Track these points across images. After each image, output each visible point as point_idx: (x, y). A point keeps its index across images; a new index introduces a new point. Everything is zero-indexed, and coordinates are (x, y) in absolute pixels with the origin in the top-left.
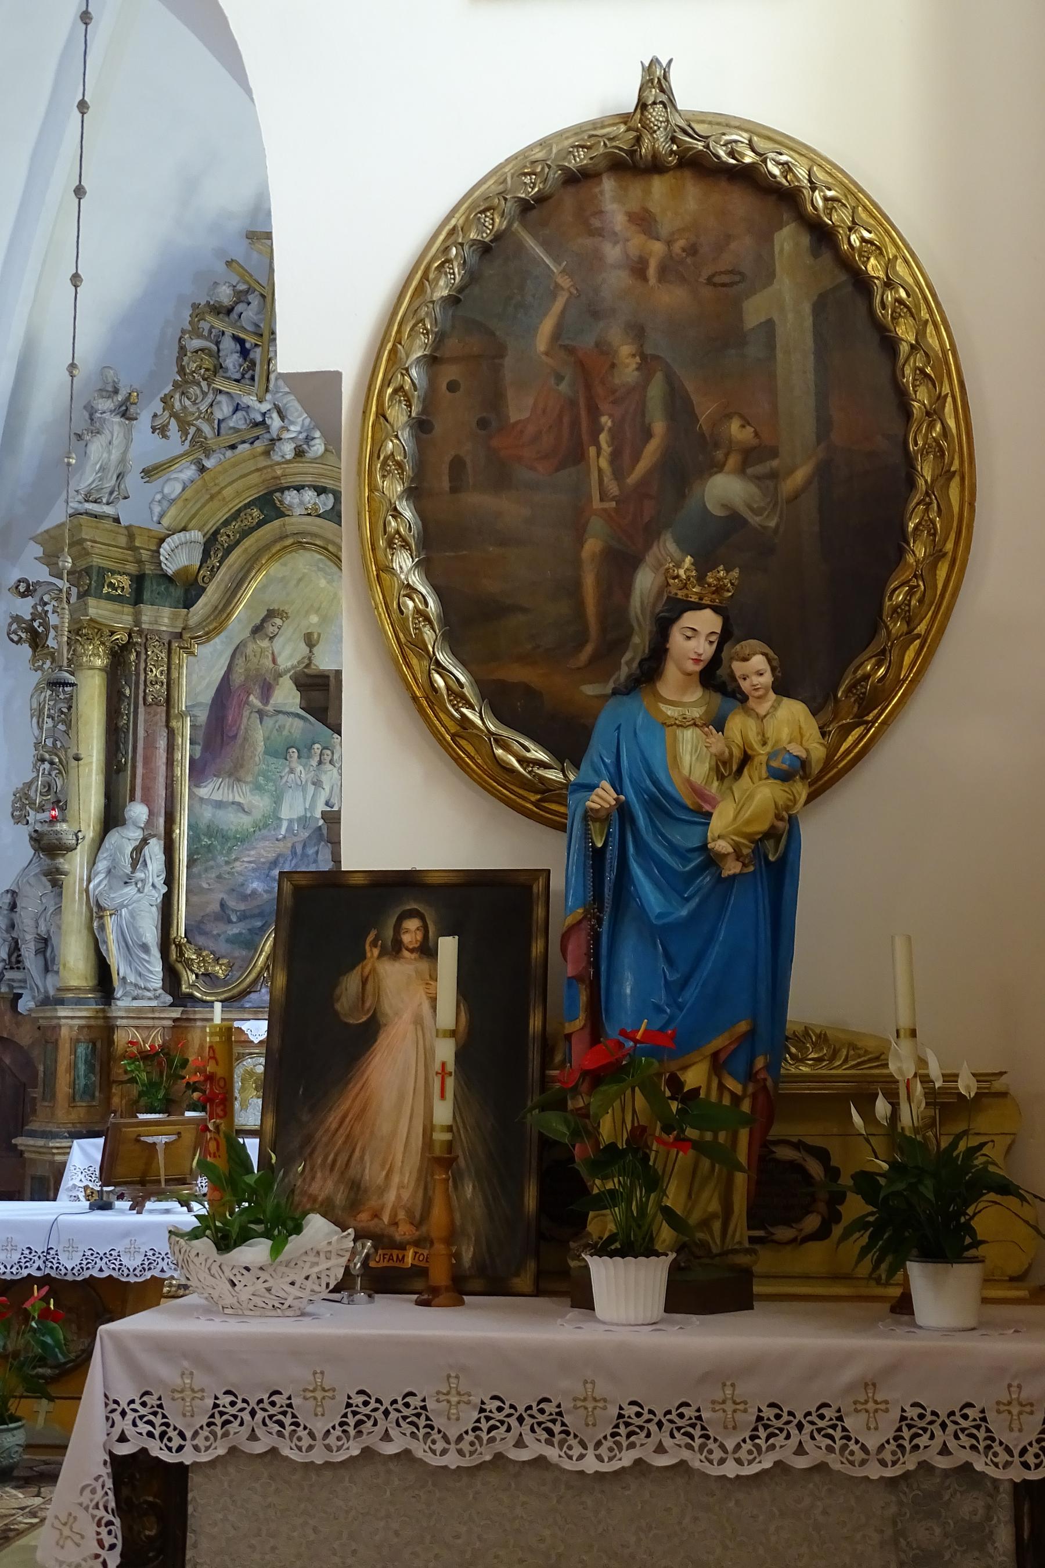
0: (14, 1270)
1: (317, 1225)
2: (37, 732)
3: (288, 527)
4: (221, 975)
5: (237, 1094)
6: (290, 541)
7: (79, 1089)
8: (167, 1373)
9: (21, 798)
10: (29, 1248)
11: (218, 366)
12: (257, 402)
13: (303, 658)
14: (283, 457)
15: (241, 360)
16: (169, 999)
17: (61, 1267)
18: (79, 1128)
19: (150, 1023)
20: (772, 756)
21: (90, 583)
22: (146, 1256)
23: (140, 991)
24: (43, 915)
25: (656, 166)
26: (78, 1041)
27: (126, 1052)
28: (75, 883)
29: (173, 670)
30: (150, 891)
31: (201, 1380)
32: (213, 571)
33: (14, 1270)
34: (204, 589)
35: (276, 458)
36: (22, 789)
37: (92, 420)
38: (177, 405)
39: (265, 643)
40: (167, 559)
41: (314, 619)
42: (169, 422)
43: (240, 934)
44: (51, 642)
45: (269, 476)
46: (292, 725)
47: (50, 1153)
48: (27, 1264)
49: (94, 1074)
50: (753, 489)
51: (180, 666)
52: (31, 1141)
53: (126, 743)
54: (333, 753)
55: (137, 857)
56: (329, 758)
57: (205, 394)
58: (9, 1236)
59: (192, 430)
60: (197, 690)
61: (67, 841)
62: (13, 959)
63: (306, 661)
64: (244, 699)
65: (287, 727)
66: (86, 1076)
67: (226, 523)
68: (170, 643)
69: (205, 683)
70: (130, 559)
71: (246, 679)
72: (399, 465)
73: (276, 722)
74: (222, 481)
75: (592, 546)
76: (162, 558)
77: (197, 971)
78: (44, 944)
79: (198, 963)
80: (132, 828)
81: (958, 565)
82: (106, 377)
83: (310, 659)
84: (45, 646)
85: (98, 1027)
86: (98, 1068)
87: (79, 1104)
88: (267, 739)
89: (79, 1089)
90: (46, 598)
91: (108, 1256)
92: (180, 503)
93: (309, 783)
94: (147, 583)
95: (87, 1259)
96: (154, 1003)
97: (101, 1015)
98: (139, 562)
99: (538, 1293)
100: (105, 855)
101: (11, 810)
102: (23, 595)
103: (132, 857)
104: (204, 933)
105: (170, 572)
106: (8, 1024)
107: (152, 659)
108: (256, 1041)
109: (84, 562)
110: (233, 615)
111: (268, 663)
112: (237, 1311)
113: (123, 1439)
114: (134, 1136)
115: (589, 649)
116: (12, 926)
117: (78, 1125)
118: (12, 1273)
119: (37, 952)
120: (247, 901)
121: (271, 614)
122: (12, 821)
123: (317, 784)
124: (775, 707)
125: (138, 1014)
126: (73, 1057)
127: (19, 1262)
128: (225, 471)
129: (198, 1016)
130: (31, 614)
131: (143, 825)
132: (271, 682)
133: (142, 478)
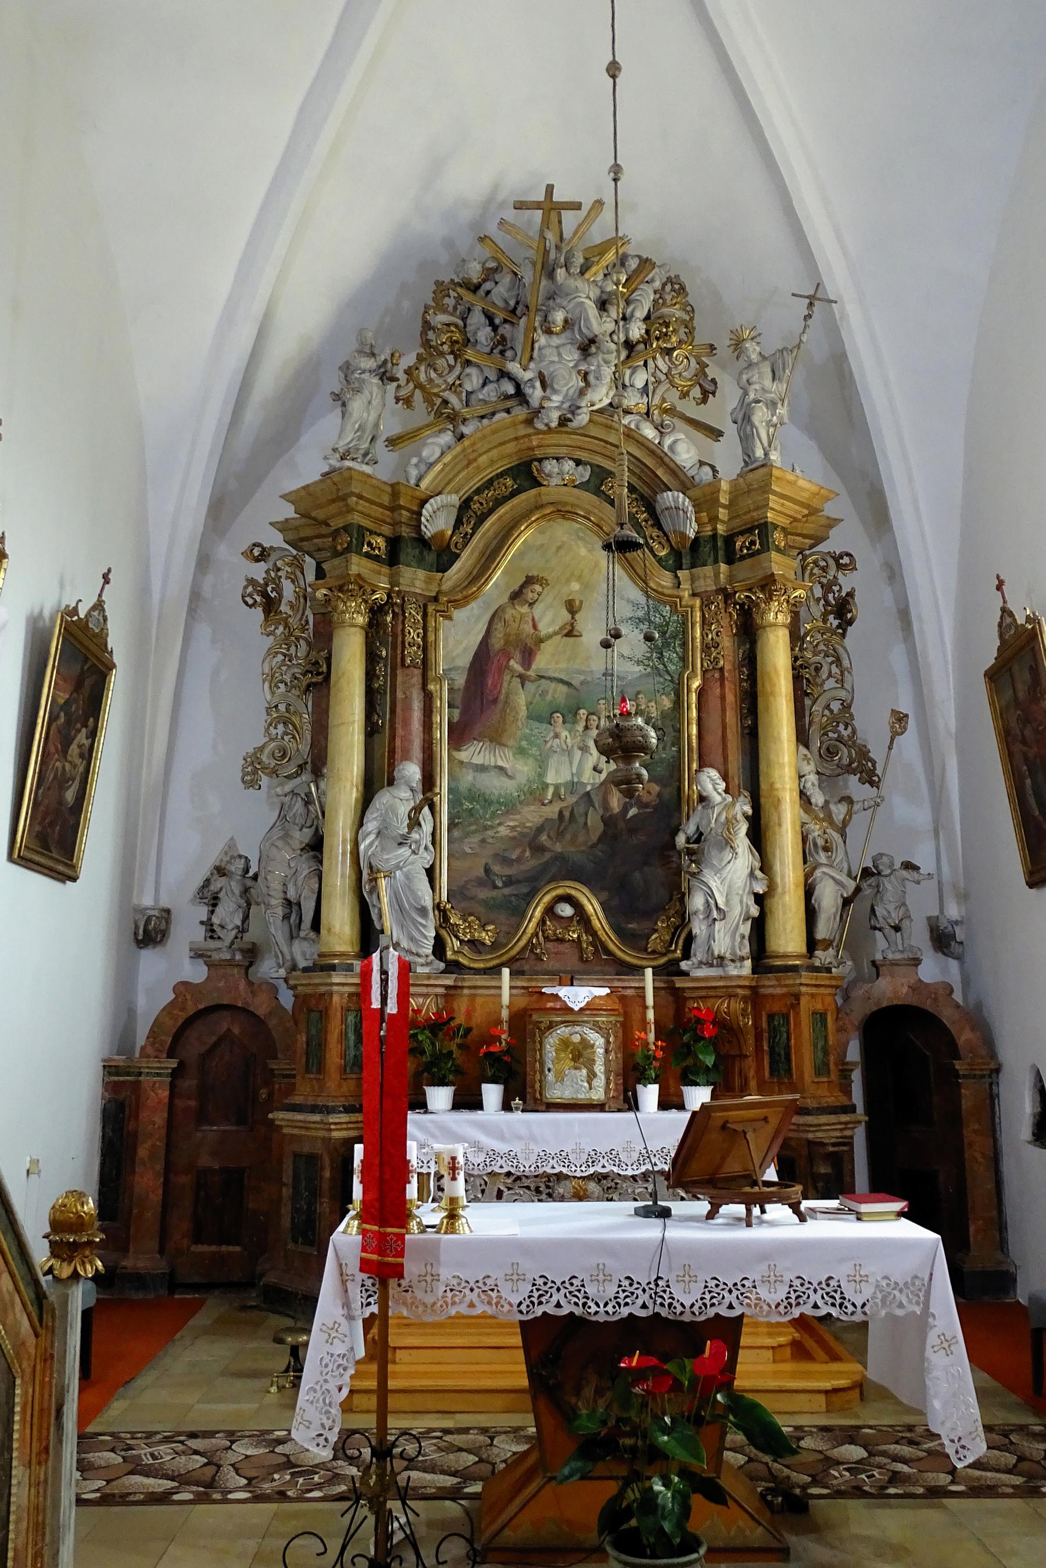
0: (610, 1308)
2: (269, 697)
9: (253, 762)
10: (628, 1278)
16: (442, 966)
17: (675, 1303)
19: (424, 990)
21: (351, 541)
22: (791, 1286)
29: (429, 634)
32: (467, 539)
33: (610, 1308)
34: (458, 556)
36: (255, 753)
38: (423, 377)
39: (525, 609)
41: (575, 586)
42: (413, 394)
44: (284, 608)
46: (555, 690)
48: (627, 1300)
51: (436, 630)
54: (599, 719)
55: (414, 823)
57: (451, 368)
58: (601, 1261)
59: (438, 401)
63: (569, 628)
67: (478, 491)
68: (425, 606)
69: (461, 647)
70: (388, 520)
76: (423, 519)
80: (404, 787)
83: (572, 625)
88: (529, 704)
90: (279, 564)
92: (438, 467)
95: (710, 1292)
102: (257, 560)
106: (243, 993)
108: (576, 1009)
111: (528, 628)
118: (607, 1312)
119: (284, 918)
121: (530, 581)
122: (242, 786)
127: (616, 1298)
128: (484, 437)
129: (466, 984)
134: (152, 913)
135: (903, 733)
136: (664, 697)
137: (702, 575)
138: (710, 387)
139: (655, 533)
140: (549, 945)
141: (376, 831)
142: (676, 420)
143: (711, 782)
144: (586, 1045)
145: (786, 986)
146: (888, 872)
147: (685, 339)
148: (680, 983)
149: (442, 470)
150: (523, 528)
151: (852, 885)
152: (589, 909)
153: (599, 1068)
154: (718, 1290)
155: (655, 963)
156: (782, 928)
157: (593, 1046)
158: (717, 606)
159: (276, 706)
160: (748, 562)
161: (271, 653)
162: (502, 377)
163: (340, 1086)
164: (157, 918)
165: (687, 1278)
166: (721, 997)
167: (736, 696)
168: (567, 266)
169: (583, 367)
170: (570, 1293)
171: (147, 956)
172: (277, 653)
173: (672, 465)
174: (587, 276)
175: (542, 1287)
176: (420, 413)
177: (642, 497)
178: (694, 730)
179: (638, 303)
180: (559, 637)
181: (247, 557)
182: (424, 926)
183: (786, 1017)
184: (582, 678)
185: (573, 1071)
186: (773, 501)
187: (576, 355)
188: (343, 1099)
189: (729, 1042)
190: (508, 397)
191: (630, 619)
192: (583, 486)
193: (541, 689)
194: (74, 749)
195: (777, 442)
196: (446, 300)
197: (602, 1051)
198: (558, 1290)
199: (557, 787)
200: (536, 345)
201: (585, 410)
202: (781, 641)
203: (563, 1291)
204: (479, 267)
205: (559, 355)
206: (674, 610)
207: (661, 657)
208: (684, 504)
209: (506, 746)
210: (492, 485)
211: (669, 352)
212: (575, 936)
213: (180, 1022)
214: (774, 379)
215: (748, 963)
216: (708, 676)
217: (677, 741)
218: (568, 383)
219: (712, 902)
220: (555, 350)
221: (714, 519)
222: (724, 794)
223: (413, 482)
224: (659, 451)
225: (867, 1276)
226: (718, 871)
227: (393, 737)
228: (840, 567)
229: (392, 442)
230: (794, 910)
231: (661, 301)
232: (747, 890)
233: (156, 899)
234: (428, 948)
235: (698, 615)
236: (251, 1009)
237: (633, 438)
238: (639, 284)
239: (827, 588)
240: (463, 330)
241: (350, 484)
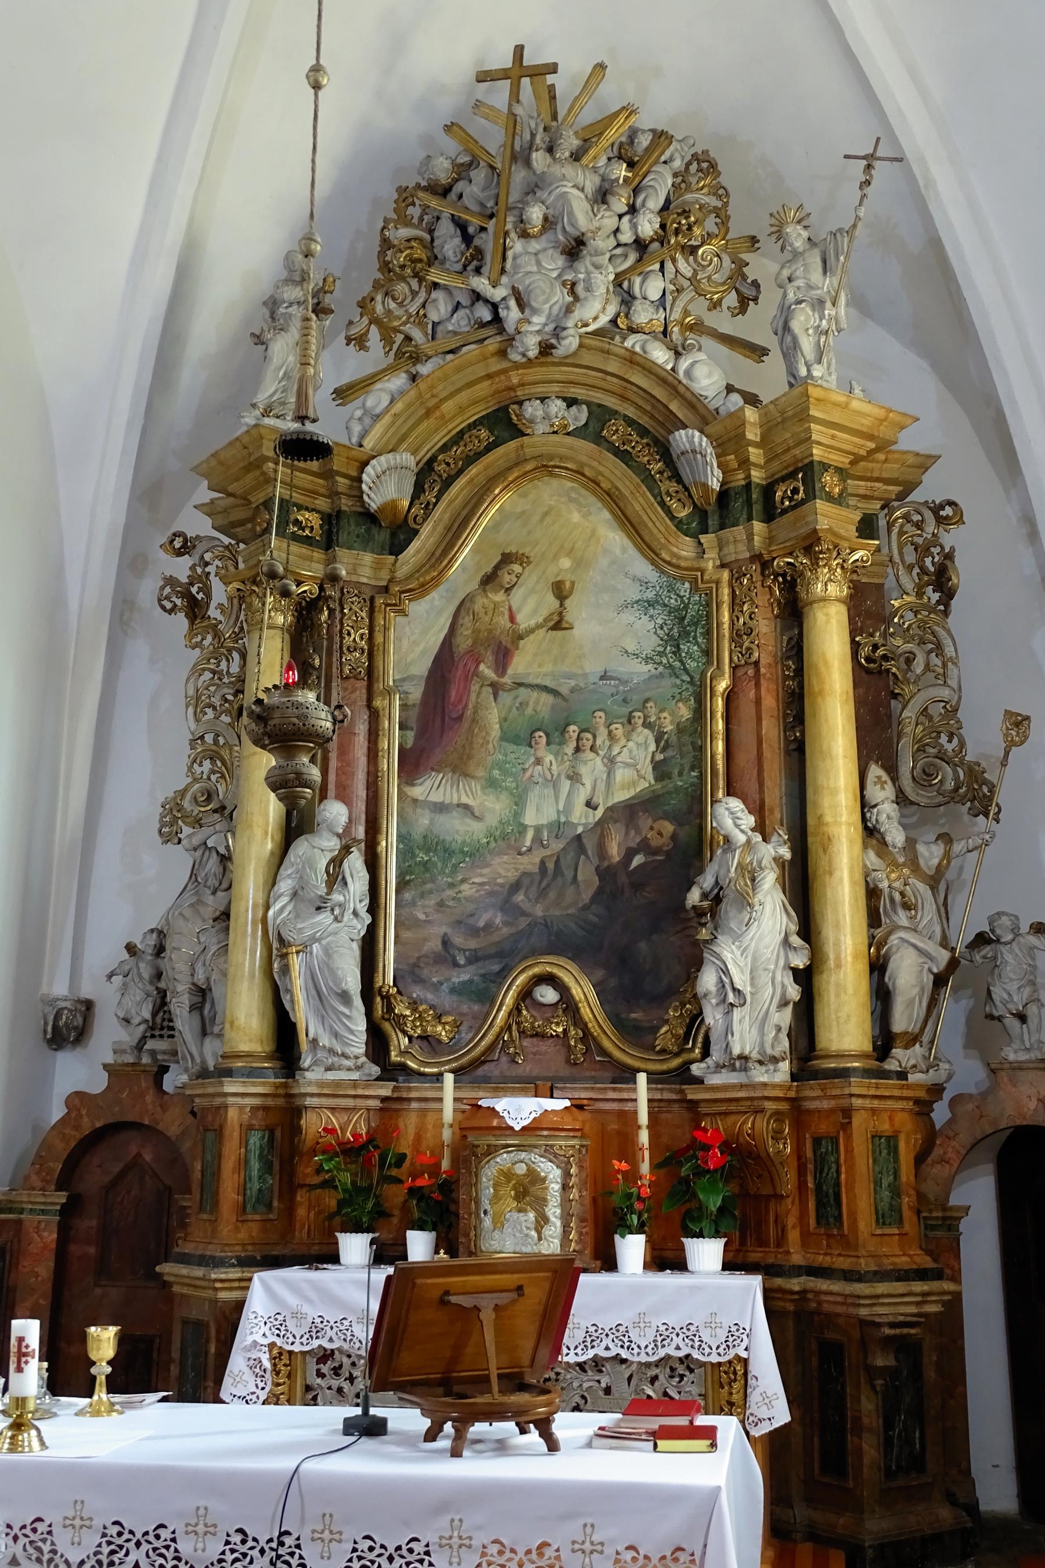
2: (193, 726)
3: (526, 450)
4: (444, 1037)
5: (486, 1204)
6: (529, 467)
7: (251, 1196)
9: (171, 809)
10: (240, 1531)
11: (432, 259)
12: (490, 287)
13: (552, 614)
14: (524, 355)
15: (463, 246)
16: (375, 1070)
18: (250, 1251)
19: (350, 1103)
23: (336, 1059)
24: (202, 958)
26: (251, 1128)
27: (318, 1143)
28: (247, 911)
30: (349, 920)
32: (429, 508)
34: (416, 532)
35: (515, 357)
36: (175, 798)
37: (273, 319)
38: (379, 309)
39: (499, 597)
40: (370, 488)
41: (566, 563)
42: (368, 330)
43: (471, 981)
44: (213, 612)
45: (501, 386)
46: (537, 702)
47: (209, 1288)
49: (271, 1175)
51: (386, 629)
52: (184, 1270)
54: (595, 737)
55: (335, 877)
56: (590, 743)
57: (414, 294)
58: (202, 1503)
59: (399, 338)
60: (409, 660)
61: (313, 721)
62: (158, 1020)
63: (556, 618)
64: (472, 669)
65: (531, 703)
66: (260, 1177)
67: (445, 448)
68: (372, 599)
69: (419, 649)
70: (323, 491)
71: (475, 643)
73: (516, 697)
74: (442, 390)
76: (364, 487)
77: (411, 1032)
78: (202, 995)
79: (413, 1021)
80: (326, 834)
82: (293, 262)
83: (560, 613)
84: (205, 617)
85: (276, 1108)
86: (276, 1167)
87: (250, 1217)
88: (504, 720)
89: (251, 1196)
90: (208, 557)
91: (404, 1552)
92: (387, 419)
93: (563, 777)
94: (343, 522)
95: (360, 1558)
96: (355, 1076)
97: (281, 1091)
98: (333, 494)
100: (289, 872)
101: (158, 826)
102: (179, 553)
103: (327, 871)
104: (419, 981)
105: (374, 506)
106: (150, 1107)
107: (350, 618)
108: (517, 1128)
109: (263, 494)
110: (452, 566)
114: (436, 1294)
116: (159, 975)
117: (250, 1248)
119: (192, 1008)
120: (479, 936)
121: (507, 559)
122: (159, 840)
123: (575, 778)
125: (334, 1091)
126: (243, 1150)
128: (446, 378)
130: (189, 577)
131: (341, 831)
132: (509, 646)
133: (334, 399)
134: (63, 1004)
135: (1022, 743)
136: (680, 705)
137: (731, 539)
138: (749, 292)
139: (673, 487)
140: (526, 1042)
141: (290, 892)
144: (534, 1178)
145: (834, 1097)
146: (1009, 937)
147: (716, 232)
148: (693, 1094)
149: (393, 423)
150: (497, 491)
151: (944, 956)
152: (576, 992)
153: (554, 1211)
154: (372, 1556)
155: (652, 1067)
156: (833, 1017)
157: (544, 1180)
158: (751, 579)
159: (202, 737)
160: (790, 516)
161: (197, 671)
162: (478, 300)
163: (237, 1230)
164: (70, 1011)
165: (326, 1535)
166: (747, 1112)
167: (777, 700)
168: (550, 150)
169: (569, 276)
170: (155, 1549)
172: (204, 670)
173: (688, 395)
174: (585, 160)
176: (376, 357)
177: (656, 442)
178: (720, 747)
179: (651, 190)
180: (542, 632)
181: (166, 551)
182: (348, 1017)
183: (835, 1141)
184: (573, 683)
185: (515, 1215)
186: (818, 432)
187: (561, 261)
188: (239, 1248)
189: (759, 1177)
190: (482, 325)
191: (637, 602)
192: (578, 433)
193: (519, 700)
195: (831, 354)
196: (411, 210)
197: (556, 1187)
198: (138, 1544)
199: (538, 829)
200: (510, 254)
201: (571, 331)
202: (834, 622)
203: (145, 1547)
204: (447, 164)
205: (538, 263)
206: (695, 588)
207: (677, 651)
208: (701, 445)
209: (473, 777)
210: (462, 438)
211: (693, 250)
212: (560, 1029)
214: (825, 272)
215: (785, 1066)
216: (740, 672)
217: (698, 763)
219: (726, 980)
220: (533, 257)
221: (745, 463)
222: (750, 833)
223: (354, 440)
224: (670, 378)
225: (602, 1544)
226: (737, 937)
228: (941, 521)
230: (850, 991)
231: (683, 185)
232: (782, 963)
235: (726, 591)
236: (160, 1127)
237: (638, 364)
238: (651, 166)
239: (924, 551)
240: (430, 245)
241: (261, 446)
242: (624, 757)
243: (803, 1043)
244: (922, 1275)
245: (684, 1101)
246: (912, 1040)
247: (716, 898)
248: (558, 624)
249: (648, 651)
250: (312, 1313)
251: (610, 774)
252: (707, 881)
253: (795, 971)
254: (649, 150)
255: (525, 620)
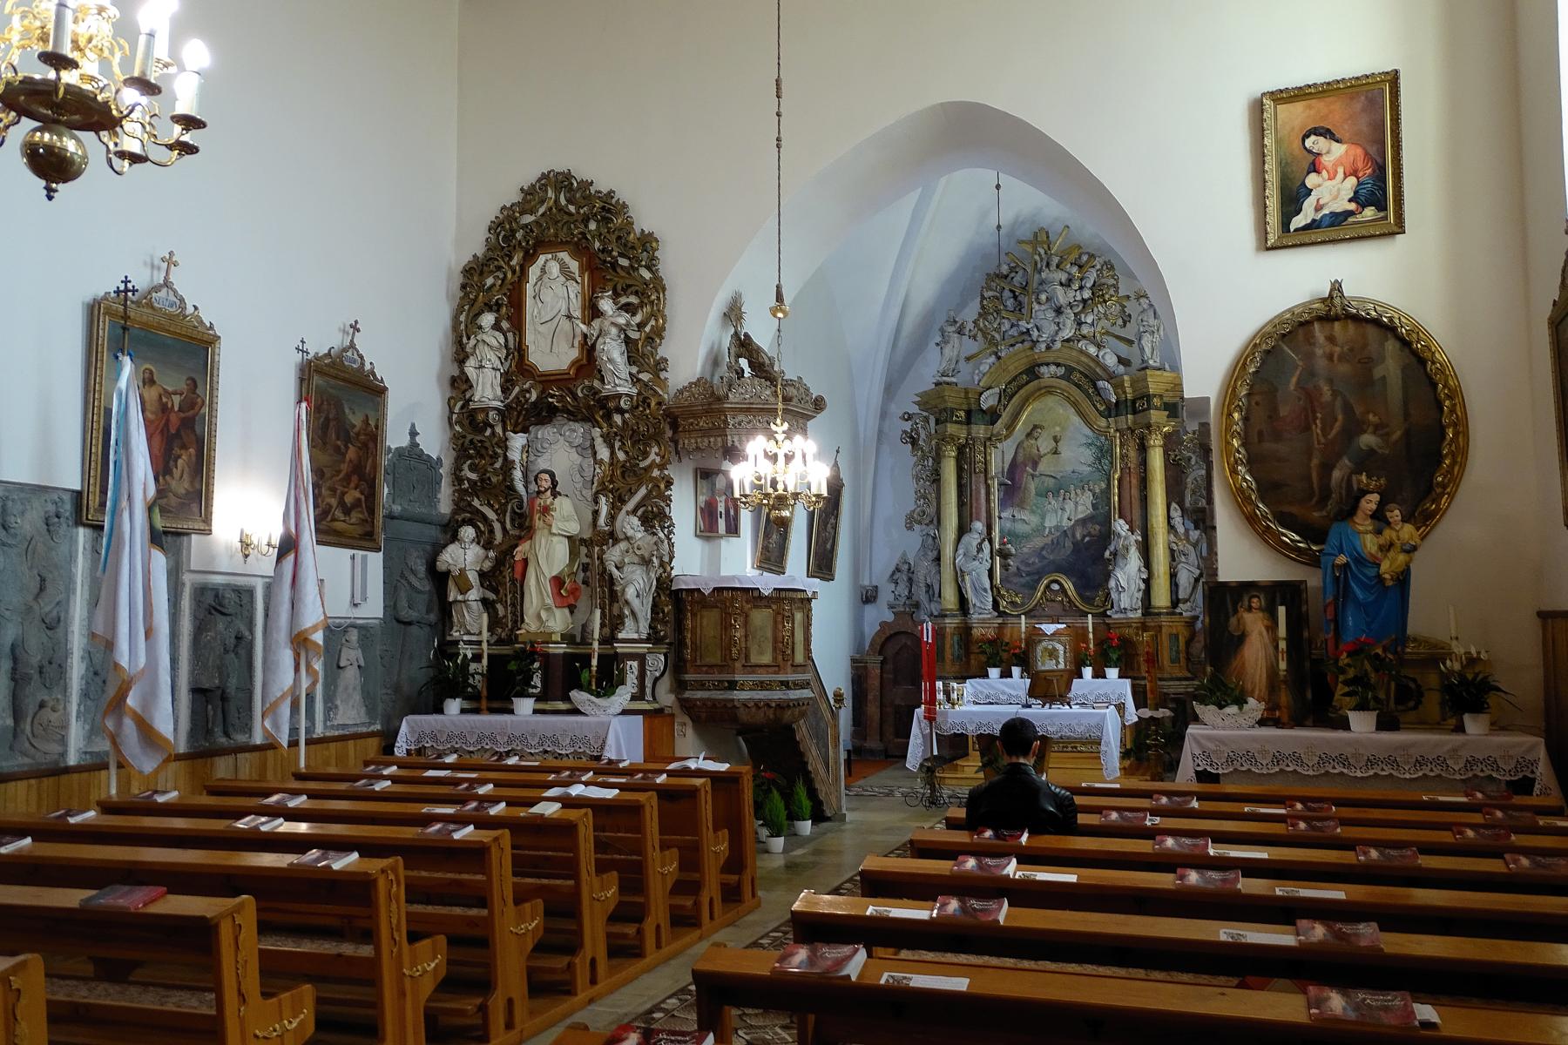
1: (1251, 701)
8: (1211, 746)
20: (1403, 544)
25: (1337, 318)
31: (1222, 748)
38: (981, 325)
39: (1033, 442)
41: (1058, 429)
50: (1379, 440)
51: (990, 454)
53: (966, 491)
55: (980, 549)
57: (995, 319)
72: (1238, 433)
75: (1315, 462)
81: (1463, 467)
94: (973, 414)
99: (1314, 726)
102: (907, 420)
104: (1009, 582)
112: (1224, 729)
113: (1198, 765)
115: (1315, 499)
121: (1035, 427)
124: (1402, 528)
125: (983, 621)
139: (1098, 398)
142: (1110, 338)
143: (1120, 526)
144: (1055, 649)
151: (1198, 572)
161: (916, 465)
171: (869, 609)
175: (979, 726)
178: (1116, 498)
187: (1053, 314)
194: (829, 526)
199: (1050, 528)
206: (1106, 439)
211: (1105, 302)
213: (883, 639)
215: (1140, 611)
218: (1049, 329)
221: (1125, 392)
227: (971, 507)
229: (968, 359)
233: (871, 582)
234: (990, 606)
242: (1082, 502)
243: (1147, 603)
244: (1186, 679)
245: (1105, 623)
246: (1186, 601)
247: (1115, 554)
248: (1056, 452)
249: (1089, 463)
250: (986, 692)
251: (1076, 507)
252: (1112, 548)
253: (1143, 580)
254: (1087, 262)
255: (1043, 451)
